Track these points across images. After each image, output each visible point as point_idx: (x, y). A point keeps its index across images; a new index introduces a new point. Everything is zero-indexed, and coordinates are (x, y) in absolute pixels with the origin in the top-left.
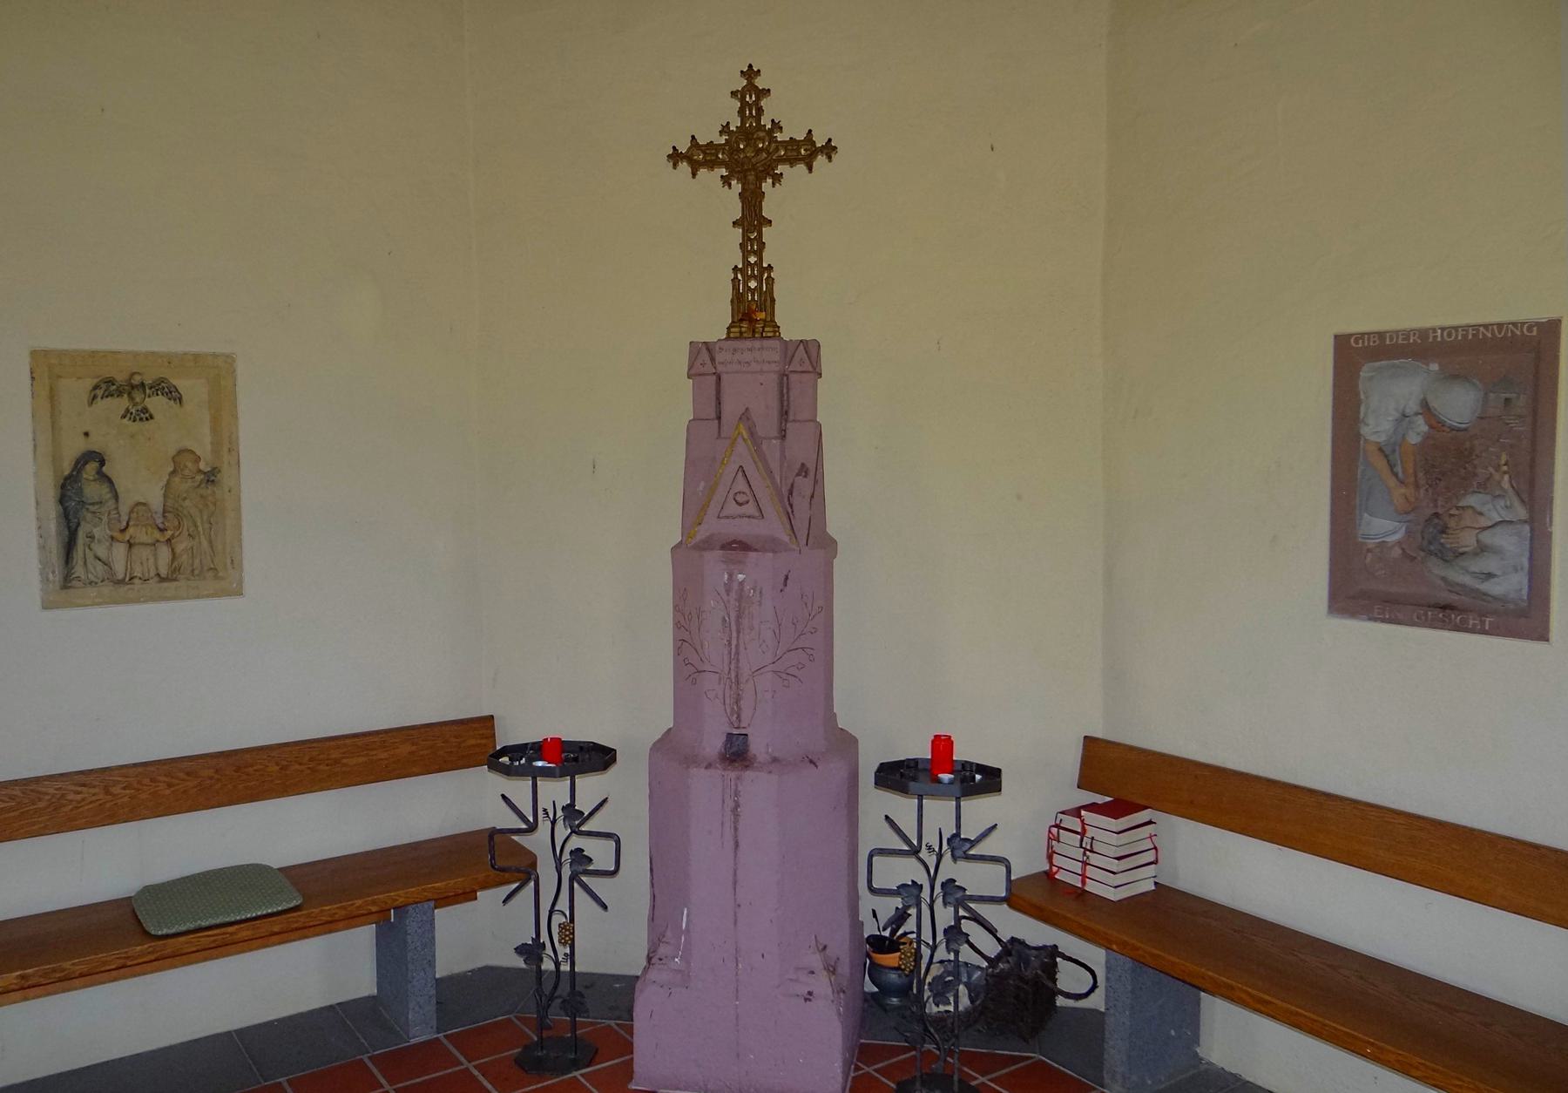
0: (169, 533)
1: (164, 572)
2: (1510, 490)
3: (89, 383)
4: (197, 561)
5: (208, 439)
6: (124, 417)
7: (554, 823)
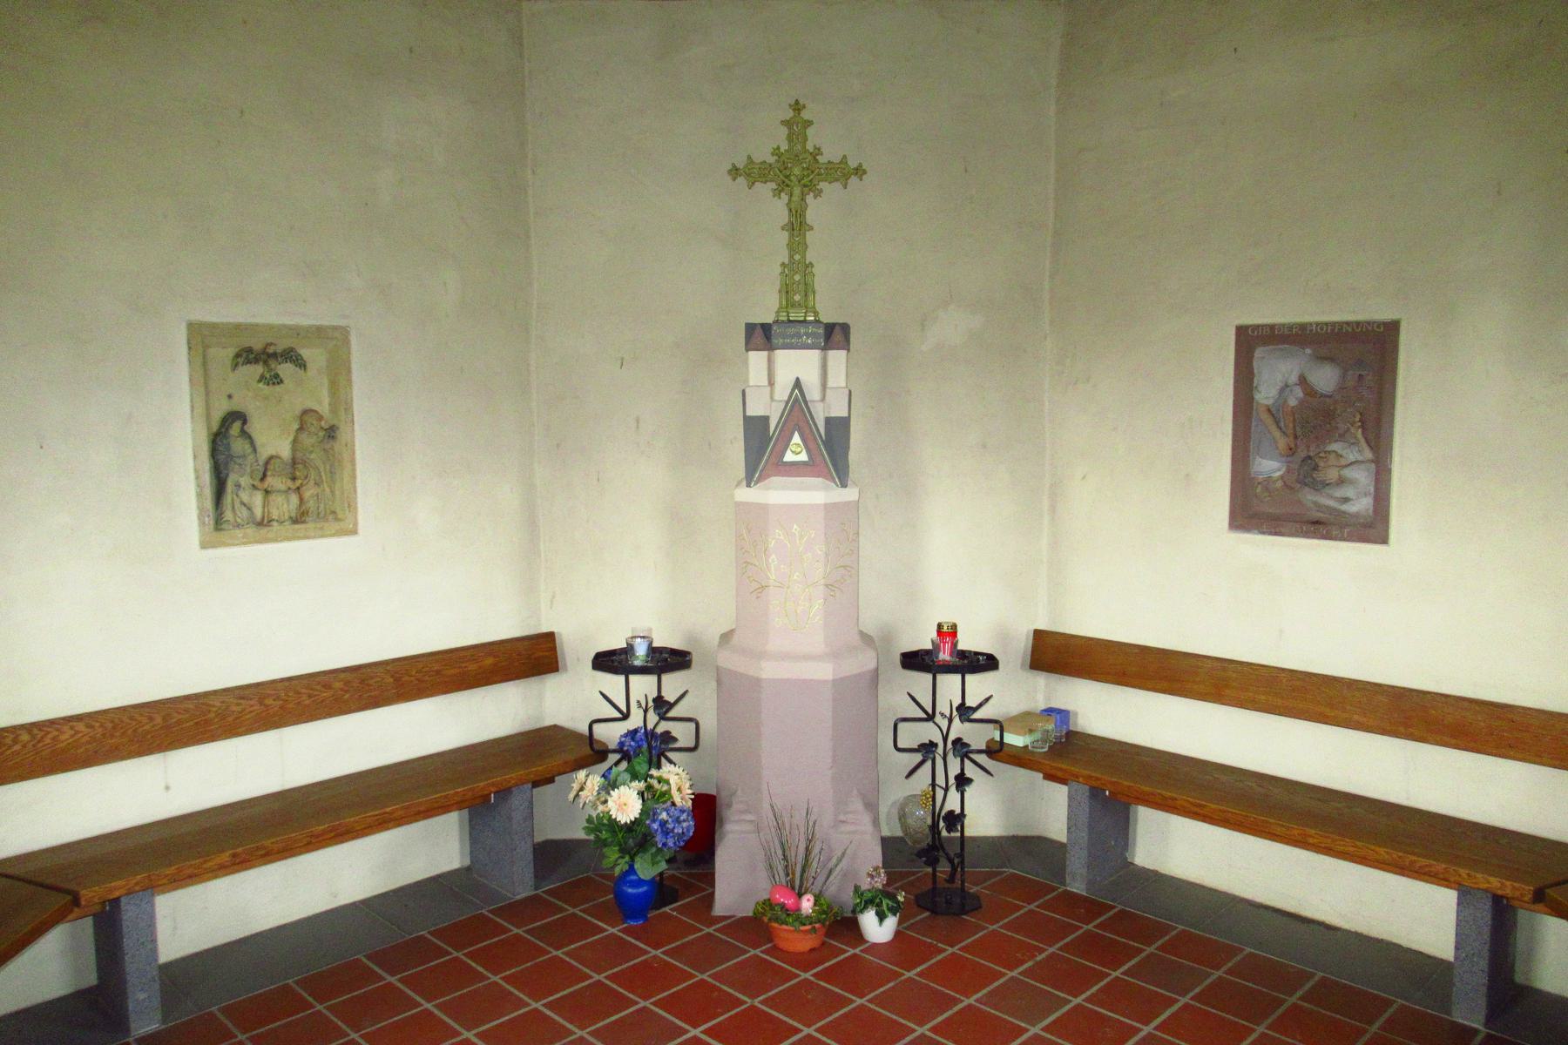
0: (298, 482)
2: (1362, 441)
3: (231, 352)
5: (326, 401)
7: (646, 711)
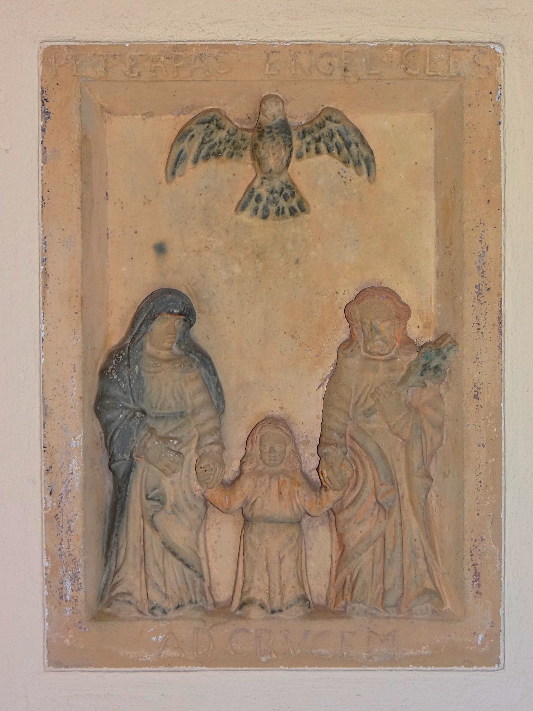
1: (319, 587)
3: (167, 126)
4: (393, 572)
5: (429, 264)
6: (242, 206)
